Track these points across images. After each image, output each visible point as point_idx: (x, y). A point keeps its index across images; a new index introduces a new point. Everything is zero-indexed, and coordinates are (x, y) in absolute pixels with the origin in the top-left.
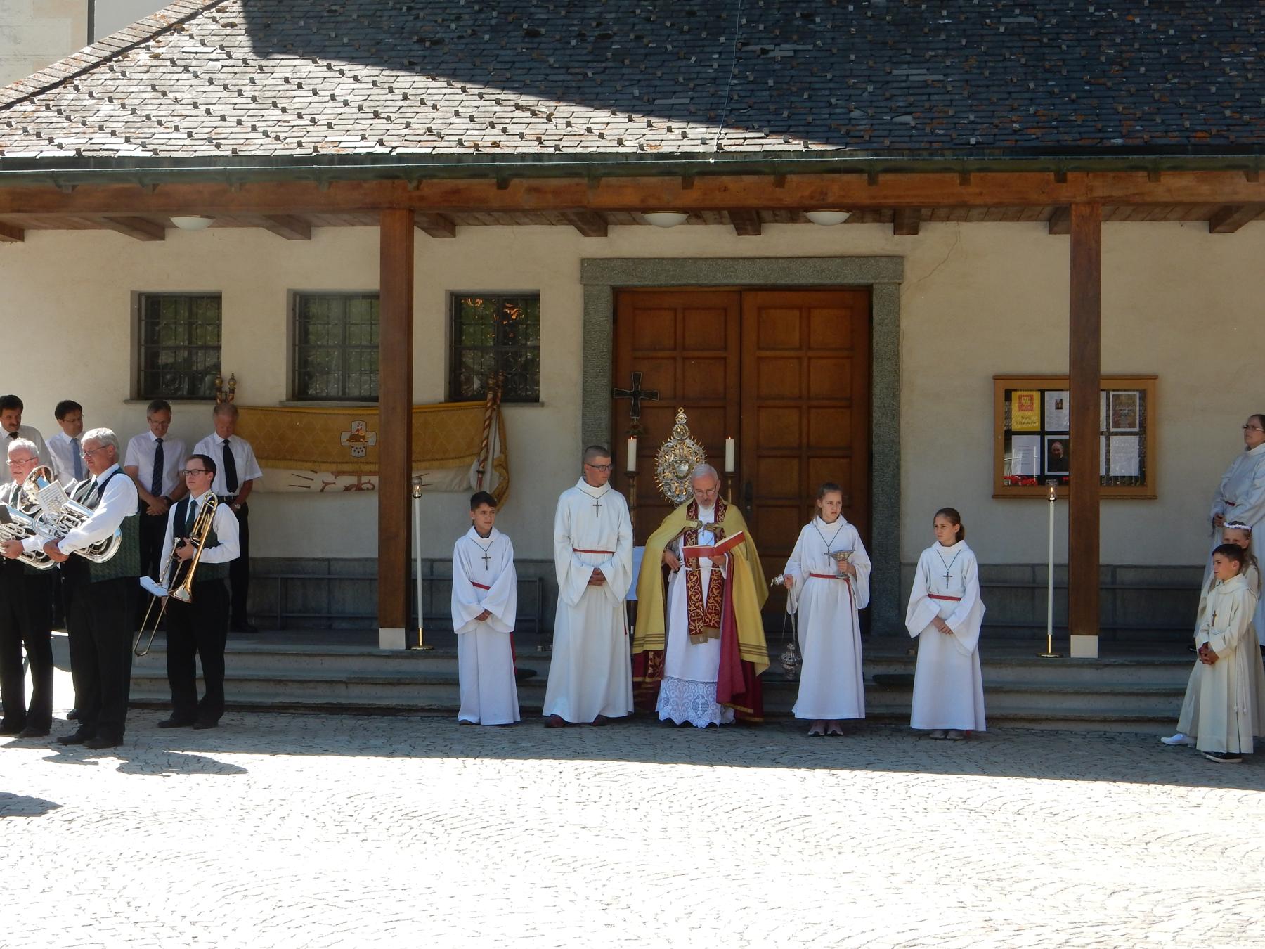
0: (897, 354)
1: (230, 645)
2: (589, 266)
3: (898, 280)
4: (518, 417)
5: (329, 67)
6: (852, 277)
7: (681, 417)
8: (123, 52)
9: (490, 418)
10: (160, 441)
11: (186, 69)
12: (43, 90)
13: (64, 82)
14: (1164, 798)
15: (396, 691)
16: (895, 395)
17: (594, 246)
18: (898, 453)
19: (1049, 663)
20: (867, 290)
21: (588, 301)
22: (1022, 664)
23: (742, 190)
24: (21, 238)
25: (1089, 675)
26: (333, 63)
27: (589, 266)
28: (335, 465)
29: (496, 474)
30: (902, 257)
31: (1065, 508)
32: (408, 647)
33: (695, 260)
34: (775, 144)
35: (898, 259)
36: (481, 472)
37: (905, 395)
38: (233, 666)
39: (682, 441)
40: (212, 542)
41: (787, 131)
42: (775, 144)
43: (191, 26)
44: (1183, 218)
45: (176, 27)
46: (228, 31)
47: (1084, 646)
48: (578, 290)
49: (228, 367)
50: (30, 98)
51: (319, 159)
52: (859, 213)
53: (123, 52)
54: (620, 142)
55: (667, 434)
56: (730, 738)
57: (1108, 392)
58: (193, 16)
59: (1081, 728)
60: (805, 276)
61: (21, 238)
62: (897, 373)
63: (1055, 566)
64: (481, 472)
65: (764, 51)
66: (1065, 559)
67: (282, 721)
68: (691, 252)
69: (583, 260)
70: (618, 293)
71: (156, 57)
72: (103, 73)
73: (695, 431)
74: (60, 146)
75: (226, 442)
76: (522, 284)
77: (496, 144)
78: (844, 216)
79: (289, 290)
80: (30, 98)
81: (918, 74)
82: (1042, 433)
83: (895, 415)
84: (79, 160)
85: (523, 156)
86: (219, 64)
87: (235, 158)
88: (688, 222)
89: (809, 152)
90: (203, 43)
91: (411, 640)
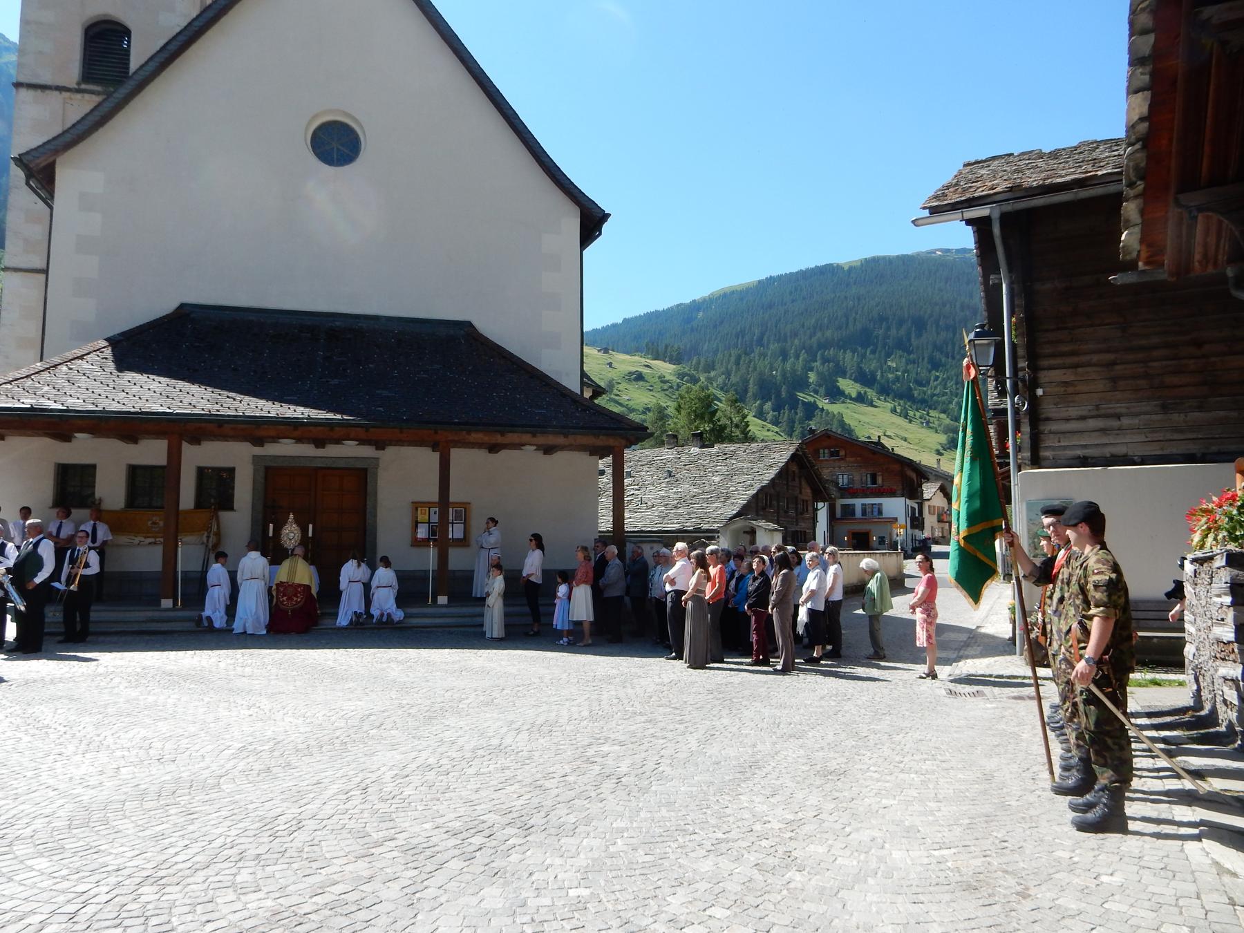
1: (92, 608)
2: (256, 459)
3: (376, 467)
4: (225, 516)
6: (359, 465)
7: (291, 516)
8: (55, 366)
11: (84, 374)
12: (17, 380)
13: (27, 377)
16: (375, 507)
17: (258, 451)
20: (365, 471)
21: (255, 471)
25: (444, 610)
27: (256, 459)
34: (330, 416)
35: (377, 459)
36: (208, 537)
38: (93, 616)
40: (87, 565)
41: (342, 413)
42: (330, 416)
45: (81, 357)
46: (104, 360)
47: (442, 600)
50: (10, 382)
51: (142, 413)
52: (362, 442)
53: (55, 366)
54: (269, 412)
55: (285, 522)
58: (88, 354)
60: (342, 464)
62: (376, 500)
69: (254, 456)
70: (267, 469)
71: (71, 369)
72: (46, 374)
73: (297, 521)
74: (23, 403)
75: (95, 524)
77: (218, 411)
78: (357, 443)
80: (10, 382)
82: (429, 523)
83: (375, 516)
84: (32, 409)
85: (229, 416)
86: (99, 374)
87: (104, 411)
88: (296, 443)
89: (344, 419)
90: (92, 365)
91: (175, 603)
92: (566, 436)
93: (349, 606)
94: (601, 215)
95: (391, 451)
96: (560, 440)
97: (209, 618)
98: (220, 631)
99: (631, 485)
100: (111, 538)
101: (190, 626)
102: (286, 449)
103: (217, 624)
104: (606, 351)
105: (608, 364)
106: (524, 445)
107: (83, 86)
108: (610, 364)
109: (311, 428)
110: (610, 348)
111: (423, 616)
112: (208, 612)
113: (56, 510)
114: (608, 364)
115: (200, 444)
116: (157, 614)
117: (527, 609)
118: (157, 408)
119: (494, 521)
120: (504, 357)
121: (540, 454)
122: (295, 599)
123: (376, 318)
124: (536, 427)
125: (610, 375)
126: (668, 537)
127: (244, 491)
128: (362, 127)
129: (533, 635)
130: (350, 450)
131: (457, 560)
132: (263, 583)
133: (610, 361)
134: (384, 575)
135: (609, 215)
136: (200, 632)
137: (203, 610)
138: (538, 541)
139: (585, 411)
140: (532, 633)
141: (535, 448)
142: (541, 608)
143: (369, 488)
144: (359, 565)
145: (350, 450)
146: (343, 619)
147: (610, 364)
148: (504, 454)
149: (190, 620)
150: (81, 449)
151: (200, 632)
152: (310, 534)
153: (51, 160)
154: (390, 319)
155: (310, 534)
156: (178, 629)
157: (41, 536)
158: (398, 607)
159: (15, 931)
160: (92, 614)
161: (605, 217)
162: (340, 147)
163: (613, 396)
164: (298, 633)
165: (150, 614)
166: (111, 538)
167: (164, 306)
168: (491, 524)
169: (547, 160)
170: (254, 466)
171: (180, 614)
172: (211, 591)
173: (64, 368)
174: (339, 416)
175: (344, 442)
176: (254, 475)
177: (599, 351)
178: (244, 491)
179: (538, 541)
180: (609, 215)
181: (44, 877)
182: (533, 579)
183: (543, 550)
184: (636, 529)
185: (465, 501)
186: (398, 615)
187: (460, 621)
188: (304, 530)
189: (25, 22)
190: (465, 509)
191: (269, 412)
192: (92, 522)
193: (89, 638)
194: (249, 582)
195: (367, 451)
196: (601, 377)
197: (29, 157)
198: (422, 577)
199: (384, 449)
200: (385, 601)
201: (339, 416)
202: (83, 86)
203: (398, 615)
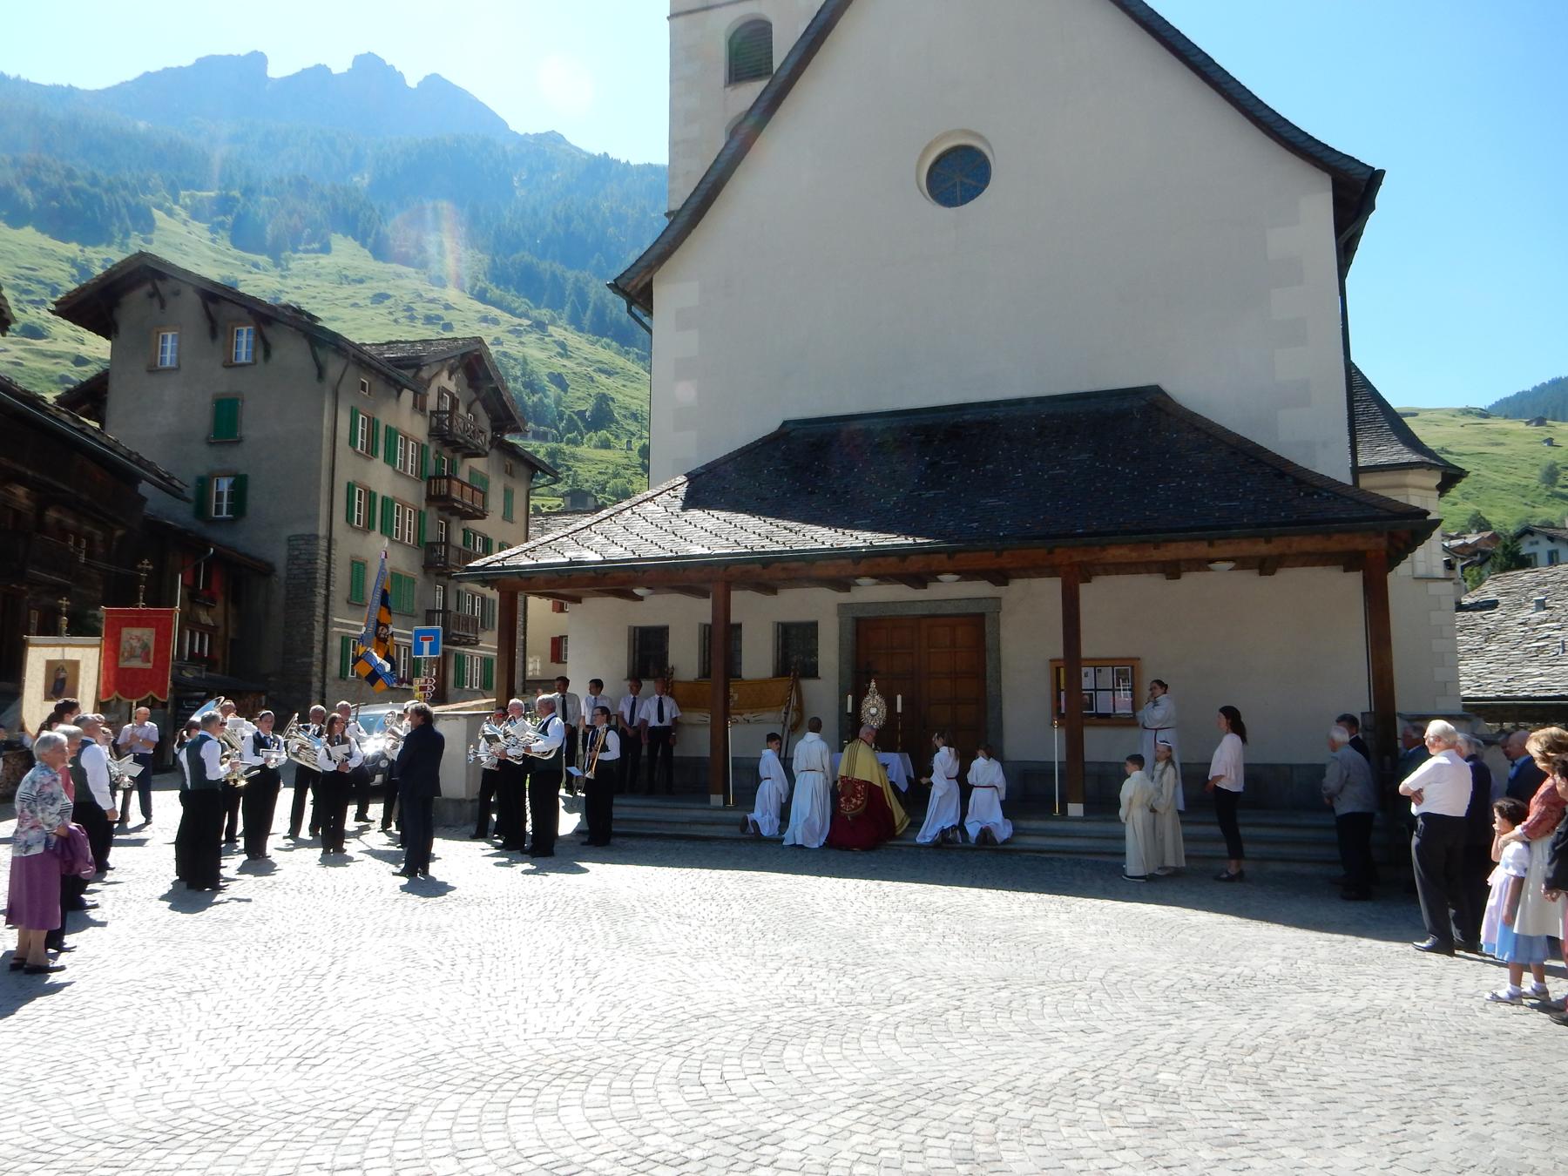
0: (999, 649)
1: (616, 801)
2: (843, 607)
4: (808, 685)
5: (844, 534)
6: (973, 609)
7: (873, 684)
9: (792, 686)
10: (634, 698)
14: (780, 884)
15: (713, 828)
16: (999, 672)
17: (843, 597)
18: (1001, 701)
19: (1055, 819)
20: (982, 616)
21: (841, 625)
22: (1042, 819)
23: (915, 564)
24: (580, 602)
25: (1077, 826)
26: (846, 531)
27: (843, 607)
28: (59, 649)
29: (794, 715)
30: (1000, 598)
31: (1063, 731)
32: (724, 804)
33: (893, 602)
34: (901, 540)
35: (998, 599)
36: (786, 713)
37: (1004, 670)
38: (618, 813)
39: (874, 697)
40: (605, 749)
41: (907, 534)
42: (901, 540)
43: (658, 499)
44: (1149, 572)
47: (1075, 809)
48: (836, 620)
49: (671, 661)
52: (967, 575)
55: (866, 693)
56: (691, 847)
57: (1113, 667)
59: (1065, 857)
60: (949, 610)
61: (580, 602)
62: (999, 659)
63: (1059, 762)
64: (786, 713)
65: (920, 495)
66: (1064, 759)
67: (682, 845)
68: (891, 599)
70: (858, 620)
73: (880, 691)
75: (660, 698)
76: (811, 618)
77: (763, 547)
78: (957, 577)
79: (700, 624)
81: (992, 502)
82: (1096, 690)
83: (999, 681)
88: (877, 584)
89: (916, 544)
91: (726, 801)
92: (1268, 541)
93: (940, 814)
94: (1367, 176)
95: (1017, 586)
96: (1201, 549)
97: (755, 823)
98: (769, 840)
99: (1546, 622)
100: (679, 714)
101: (734, 831)
102: (870, 593)
103: (765, 832)
104: (1541, 422)
105: (1545, 441)
106: (1213, 561)
108: (1550, 442)
109: (880, 560)
110: (1550, 416)
111: (1040, 834)
112: (756, 815)
113: (628, 683)
114: (1545, 441)
115: (776, 594)
116: (706, 813)
117: (1216, 830)
118: (697, 550)
119: (1163, 685)
120: (1197, 429)
121: (1250, 578)
122: (854, 800)
123: (1021, 402)
124: (1214, 529)
125: (1549, 458)
126: (1502, 705)
127: (829, 654)
128: (989, 146)
129: (1225, 880)
130: (950, 590)
131: (1099, 745)
132: (822, 777)
133: (1548, 436)
134: (984, 770)
135: (1382, 173)
136: (745, 840)
137: (752, 811)
138: (1234, 721)
139: (1312, 494)
140: (1225, 876)
141: (1231, 565)
142: (1242, 831)
143: (989, 640)
144: (1348, 720)
145: (950, 590)
146: (928, 833)
147: (1550, 442)
148: (1190, 580)
149: (731, 823)
150: (655, 609)
151: (745, 840)
152: (899, 709)
153: (647, 279)
154: (1039, 400)
155: (899, 709)
156: (722, 835)
157: (554, 714)
158: (1006, 815)
159: (626, 1174)
160: (615, 810)
161: (1374, 178)
162: (966, 181)
163: (1557, 489)
164: (863, 850)
165: (697, 813)
166: (679, 714)
167: (770, 425)
168: (1159, 690)
169: (1265, 113)
170: (840, 618)
171: (732, 814)
172: (174, 839)
173: (629, 512)
174: (910, 540)
175: (940, 577)
176: (840, 629)
177: (1528, 423)
178: (829, 654)
179: (1234, 721)
180: (1382, 173)
181: (847, 1063)
182: (1223, 785)
183: (1244, 740)
184: (1552, 694)
185: (1133, 654)
186: (1003, 831)
187: (1097, 844)
188: (891, 704)
189: (673, 144)
190: (1132, 667)
191: (823, 543)
192: (657, 697)
193: (616, 841)
194: (804, 773)
195: (980, 589)
196: (1534, 462)
197: (624, 281)
198: (1045, 770)
199: (1007, 585)
200: (987, 811)
201: (910, 540)
203: (1003, 831)
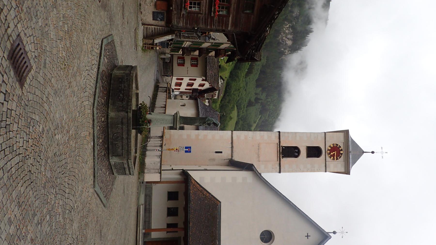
17: (182, 238)
107: (281, 147)
202: (281, 147)
